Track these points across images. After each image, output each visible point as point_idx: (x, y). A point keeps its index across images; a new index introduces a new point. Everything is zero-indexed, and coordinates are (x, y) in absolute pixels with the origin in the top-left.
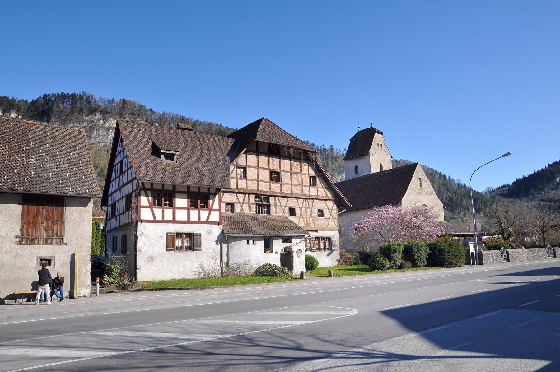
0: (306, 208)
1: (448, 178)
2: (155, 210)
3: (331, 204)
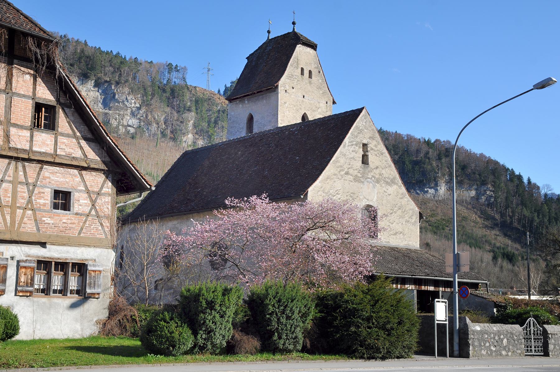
0: (15, 183)
1: (525, 181)
3: (98, 181)
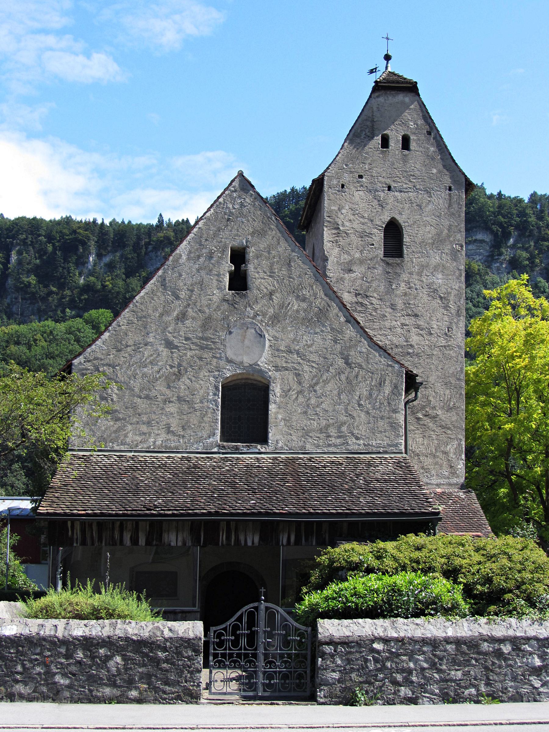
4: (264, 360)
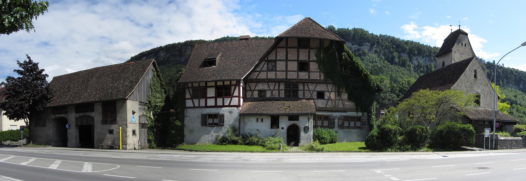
2: (194, 100)
4: (480, 91)
